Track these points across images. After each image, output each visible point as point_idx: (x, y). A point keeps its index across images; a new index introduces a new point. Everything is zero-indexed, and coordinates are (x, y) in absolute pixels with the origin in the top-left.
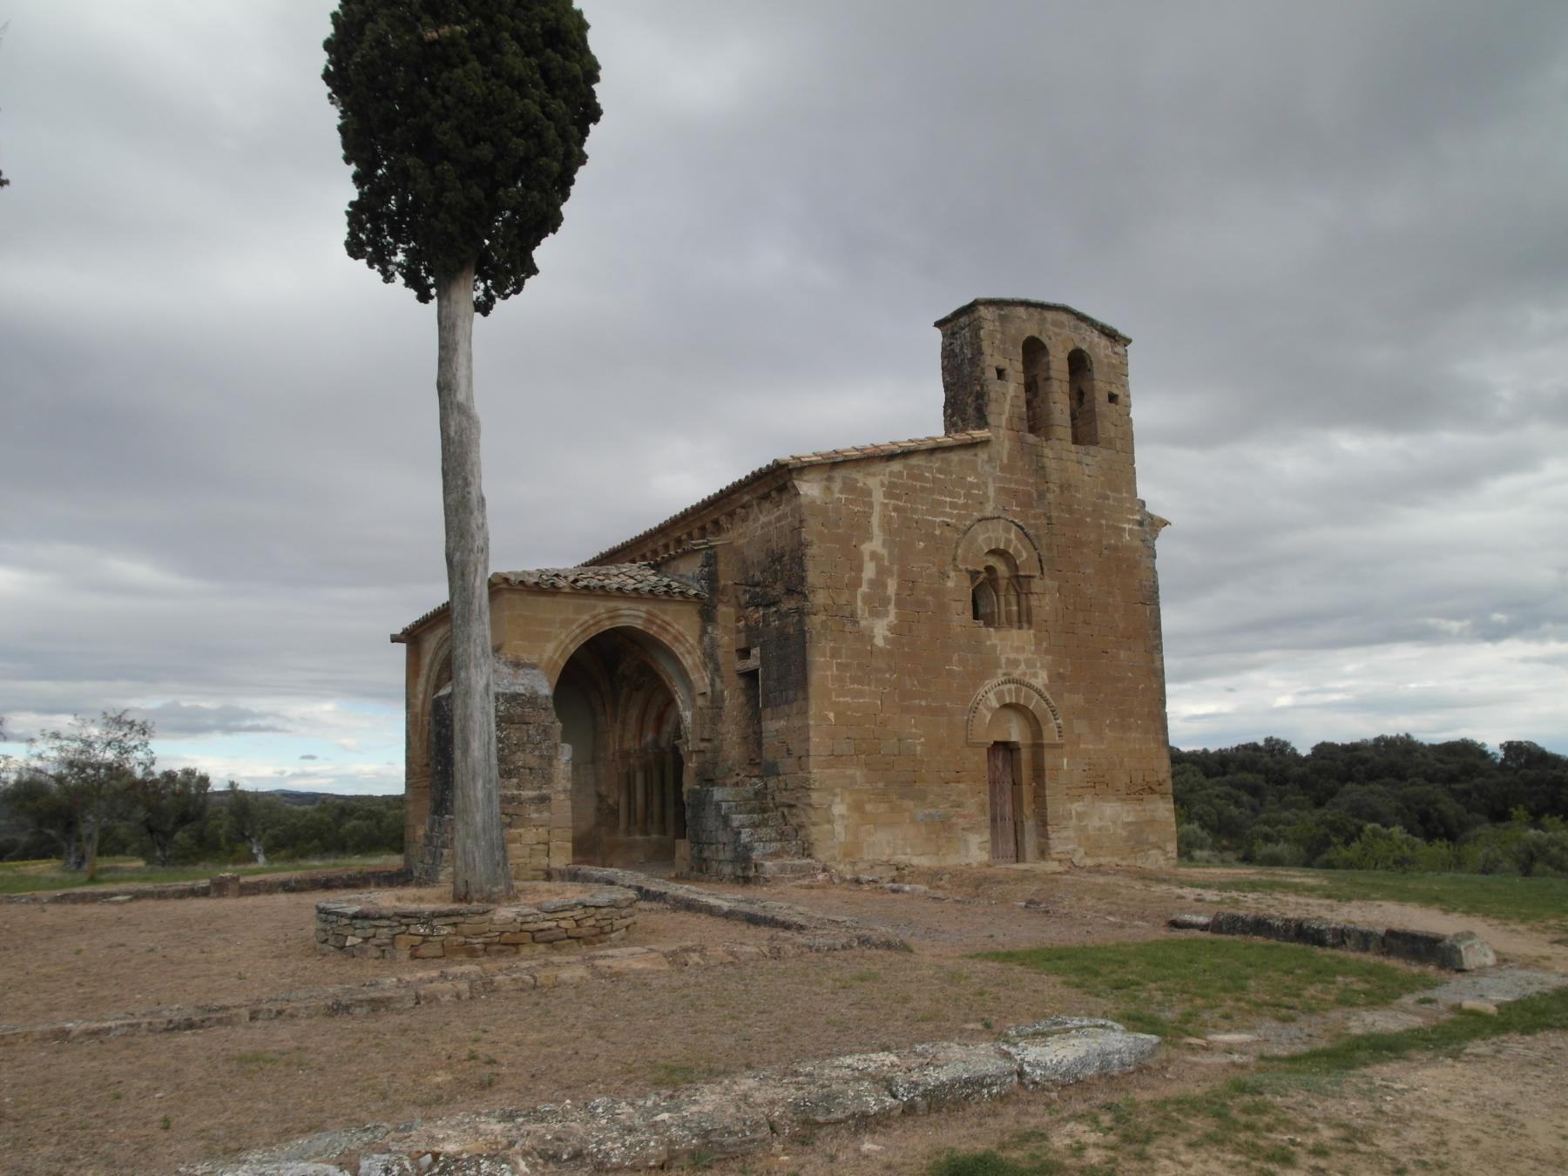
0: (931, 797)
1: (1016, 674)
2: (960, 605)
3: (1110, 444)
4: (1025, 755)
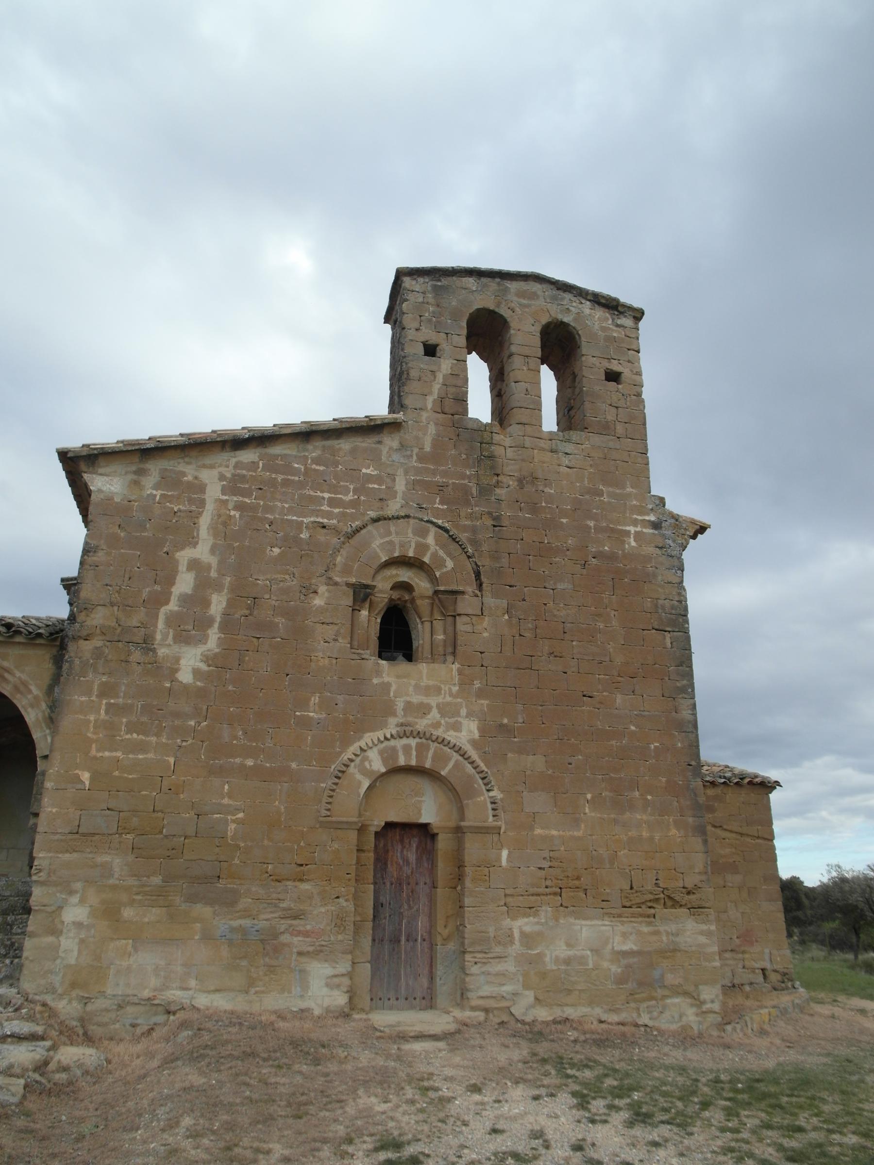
0: (245, 902)
1: (422, 724)
2: (330, 631)
3: (606, 429)
4: (443, 843)
